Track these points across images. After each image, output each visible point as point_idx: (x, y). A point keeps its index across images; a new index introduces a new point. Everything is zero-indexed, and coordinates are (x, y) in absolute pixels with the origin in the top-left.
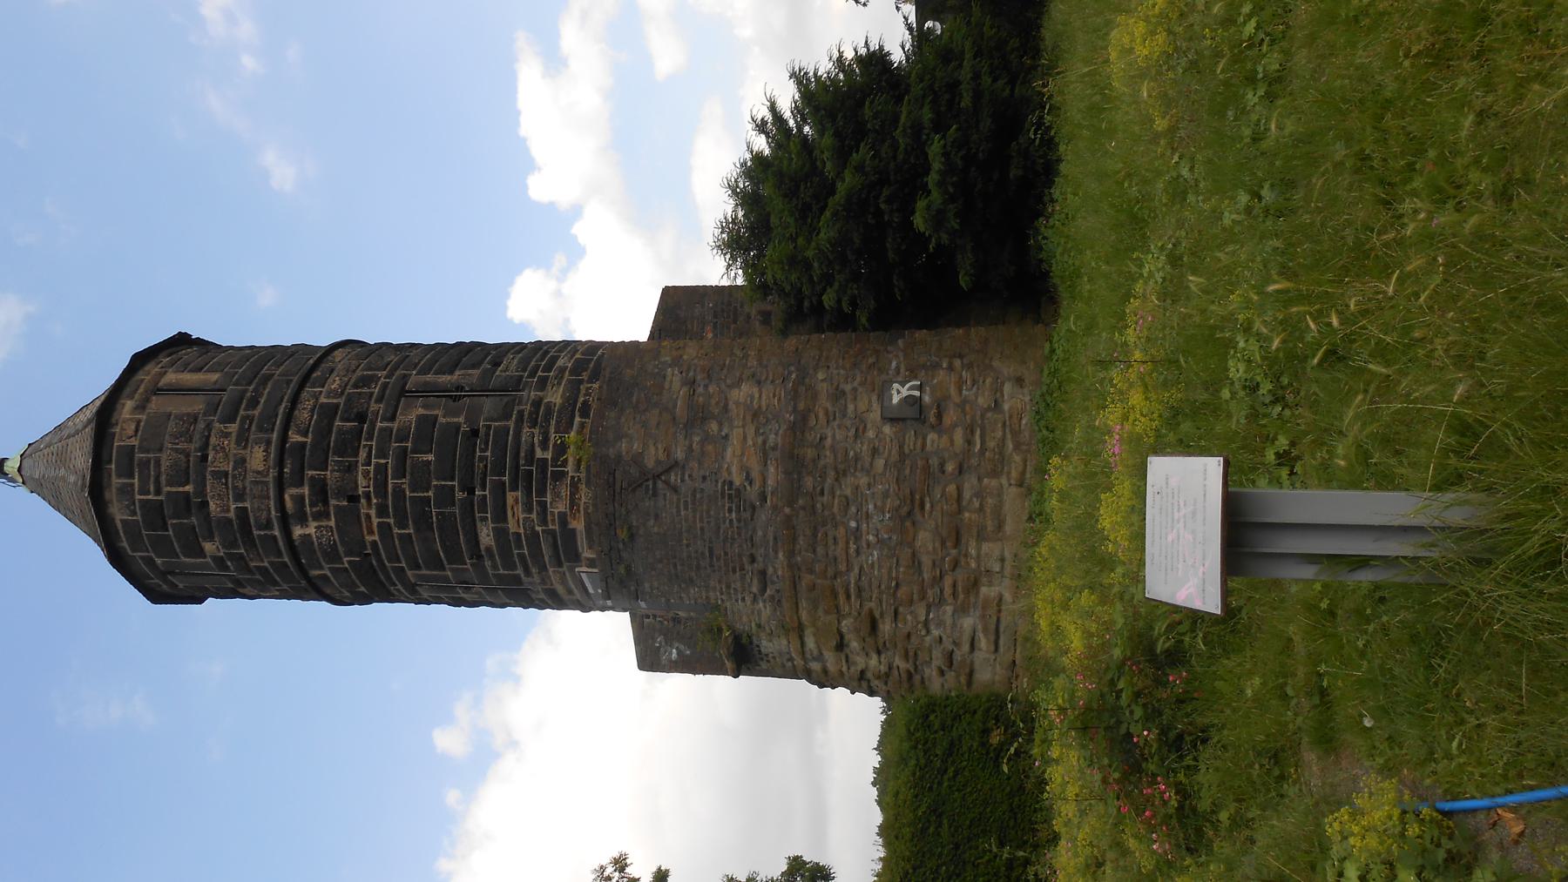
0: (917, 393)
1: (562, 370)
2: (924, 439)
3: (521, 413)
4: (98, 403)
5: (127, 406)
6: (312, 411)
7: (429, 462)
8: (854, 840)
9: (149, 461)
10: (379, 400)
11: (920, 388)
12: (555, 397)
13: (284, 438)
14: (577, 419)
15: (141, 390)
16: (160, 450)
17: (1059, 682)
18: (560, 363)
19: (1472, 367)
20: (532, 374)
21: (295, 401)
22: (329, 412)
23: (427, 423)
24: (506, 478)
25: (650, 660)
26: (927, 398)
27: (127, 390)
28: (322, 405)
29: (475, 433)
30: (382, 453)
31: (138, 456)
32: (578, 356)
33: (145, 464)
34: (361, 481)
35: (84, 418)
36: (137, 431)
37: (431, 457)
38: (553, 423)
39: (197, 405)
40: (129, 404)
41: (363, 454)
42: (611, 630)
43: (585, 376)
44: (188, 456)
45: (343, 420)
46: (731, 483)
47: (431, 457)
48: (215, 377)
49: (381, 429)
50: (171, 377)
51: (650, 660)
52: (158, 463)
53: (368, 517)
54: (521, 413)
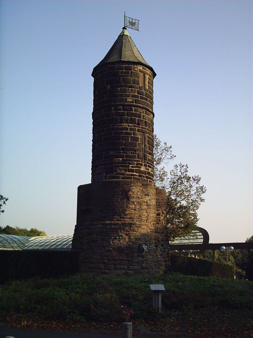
0: (145, 251)
1: (148, 170)
2: (136, 253)
3: (139, 161)
4: (146, 64)
5: (141, 68)
6: (140, 112)
7: (129, 140)
8: (15, 216)
9: (129, 74)
10: (142, 128)
11: (146, 252)
12: (143, 169)
13: (134, 106)
14: (138, 174)
15: (144, 70)
16: (131, 77)
17: (94, 296)
18: (150, 169)
19: (62, 300)
20: (147, 163)
21: (143, 108)
22: (139, 116)
23: (137, 139)
24: (125, 158)
25: (81, 188)
26: (144, 253)
27: (144, 67)
28: (141, 114)
29: (135, 151)
30: (130, 129)
31: (130, 71)
32: (151, 172)
33: (128, 73)
34: (124, 124)
35: (136, 54)
36: (135, 71)
37: (130, 141)
38: (137, 168)
39: (141, 85)
40: (141, 68)
41: (130, 125)
42: (87, 180)
43: (147, 175)
44: (130, 83)
45: (138, 119)
46: (126, 211)
47: (130, 141)
48: (147, 88)
49: (136, 129)
50: (147, 77)
51: (81, 188)
52: (128, 76)
53: (116, 126)
54: (139, 161)
